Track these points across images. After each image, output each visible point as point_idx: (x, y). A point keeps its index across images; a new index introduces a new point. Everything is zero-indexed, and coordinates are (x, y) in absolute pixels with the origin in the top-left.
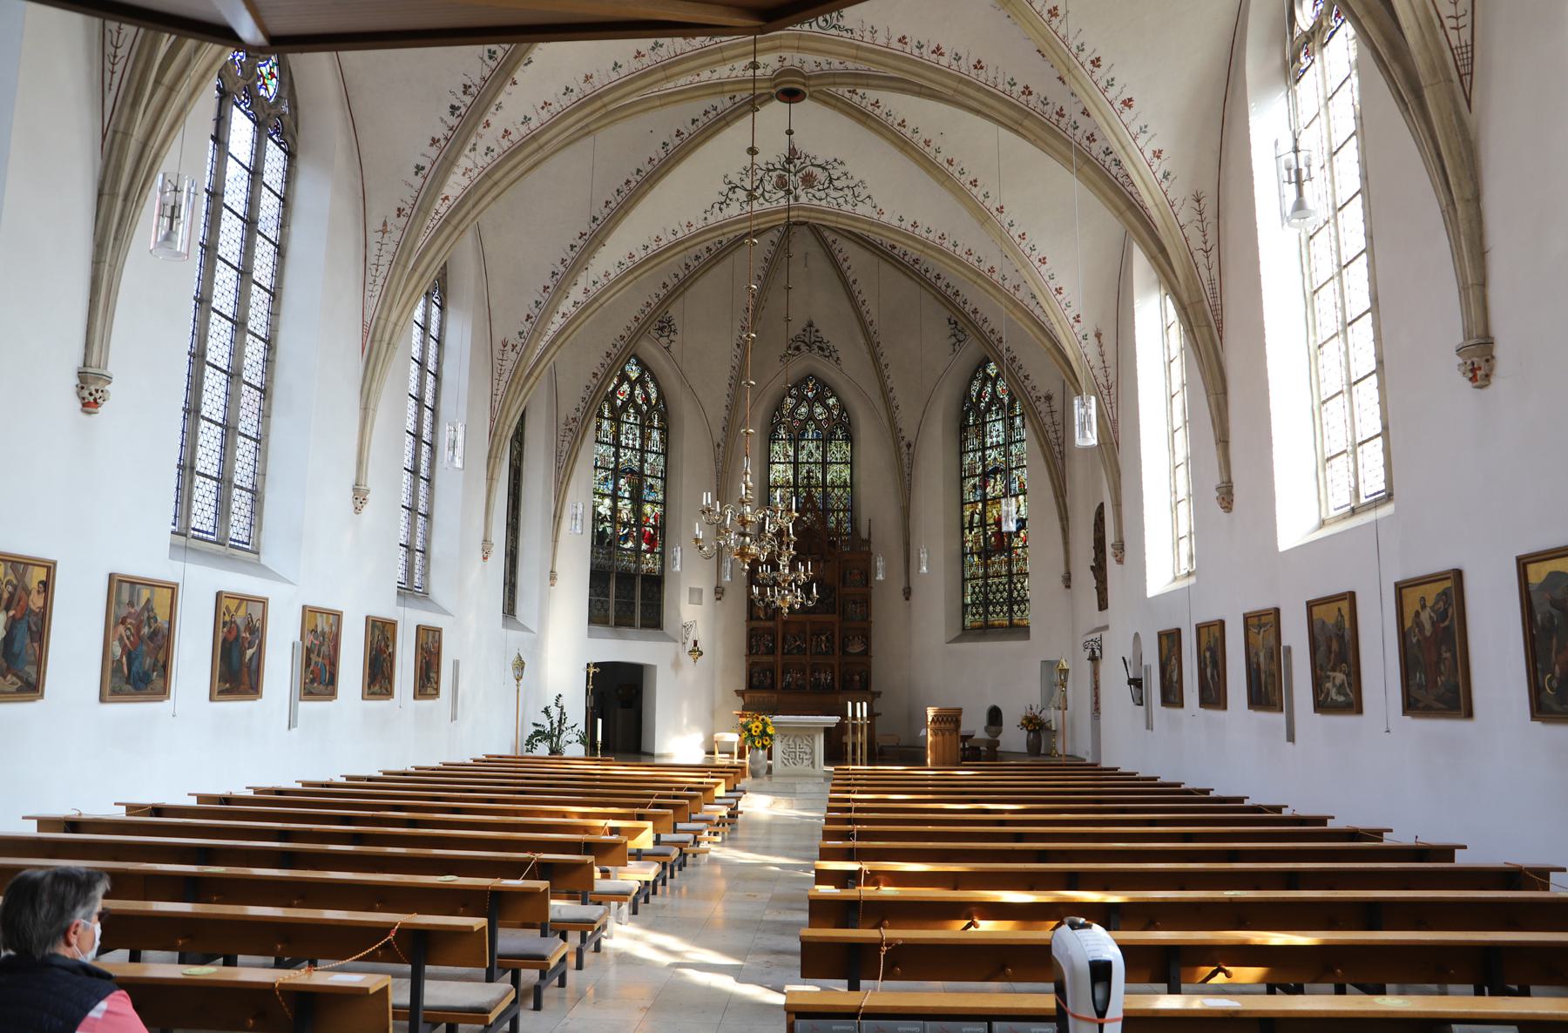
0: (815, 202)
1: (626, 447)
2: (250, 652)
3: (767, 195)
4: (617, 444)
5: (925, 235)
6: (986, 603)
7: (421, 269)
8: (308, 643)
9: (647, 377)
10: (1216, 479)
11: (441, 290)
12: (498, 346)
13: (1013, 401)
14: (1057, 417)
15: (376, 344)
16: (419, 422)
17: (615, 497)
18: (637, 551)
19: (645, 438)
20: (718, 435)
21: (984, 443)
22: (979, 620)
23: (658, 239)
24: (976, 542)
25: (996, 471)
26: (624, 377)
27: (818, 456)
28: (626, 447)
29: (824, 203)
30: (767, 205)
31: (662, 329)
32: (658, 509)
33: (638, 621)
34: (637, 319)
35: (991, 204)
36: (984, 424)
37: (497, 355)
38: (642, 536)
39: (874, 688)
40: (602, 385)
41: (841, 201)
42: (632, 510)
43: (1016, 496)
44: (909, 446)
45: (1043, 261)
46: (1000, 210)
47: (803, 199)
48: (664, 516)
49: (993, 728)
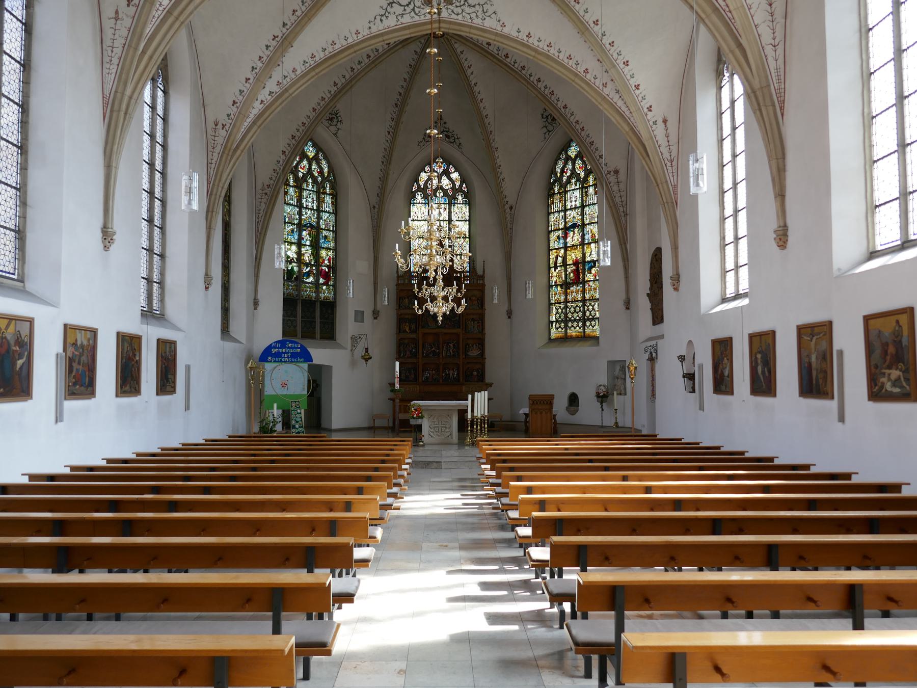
0: (454, 16)
1: (307, 208)
2: (20, 362)
3: (417, 10)
4: (300, 206)
5: (536, 43)
6: (566, 321)
7: (149, 53)
8: (69, 354)
9: (321, 156)
10: (773, 224)
11: (163, 75)
12: (211, 125)
13: (587, 176)
14: (622, 186)
15: (116, 114)
16: (151, 238)
17: (300, 245)
18: (316, 284)
19: (320, 201)
20: (374, 200)
21: (565, 206)
22: (561, 332)
23: (334, 43)
24: (560, 276)
25: (574, 226)
26: (304, 156)
27: (445, 216)
28: (307, 208)
29: (460, 17)
30: (417, 18)
31: (331, 119)
32: (331, 254)
33: (318, 335)
34: (314, 110)
35: (589, 18)
36: (566, 192)
37: (210, 131)
38: (320, 273)
39: (487, 380)
40: (289, 161)
41: (473, 15)
42: (312, 254)
43: (589, 244)
44: (511, 208)
45: (626, 63)
46: (596, 23)
47: (444, 14)
48: (335, 259)
49: (572, 408)
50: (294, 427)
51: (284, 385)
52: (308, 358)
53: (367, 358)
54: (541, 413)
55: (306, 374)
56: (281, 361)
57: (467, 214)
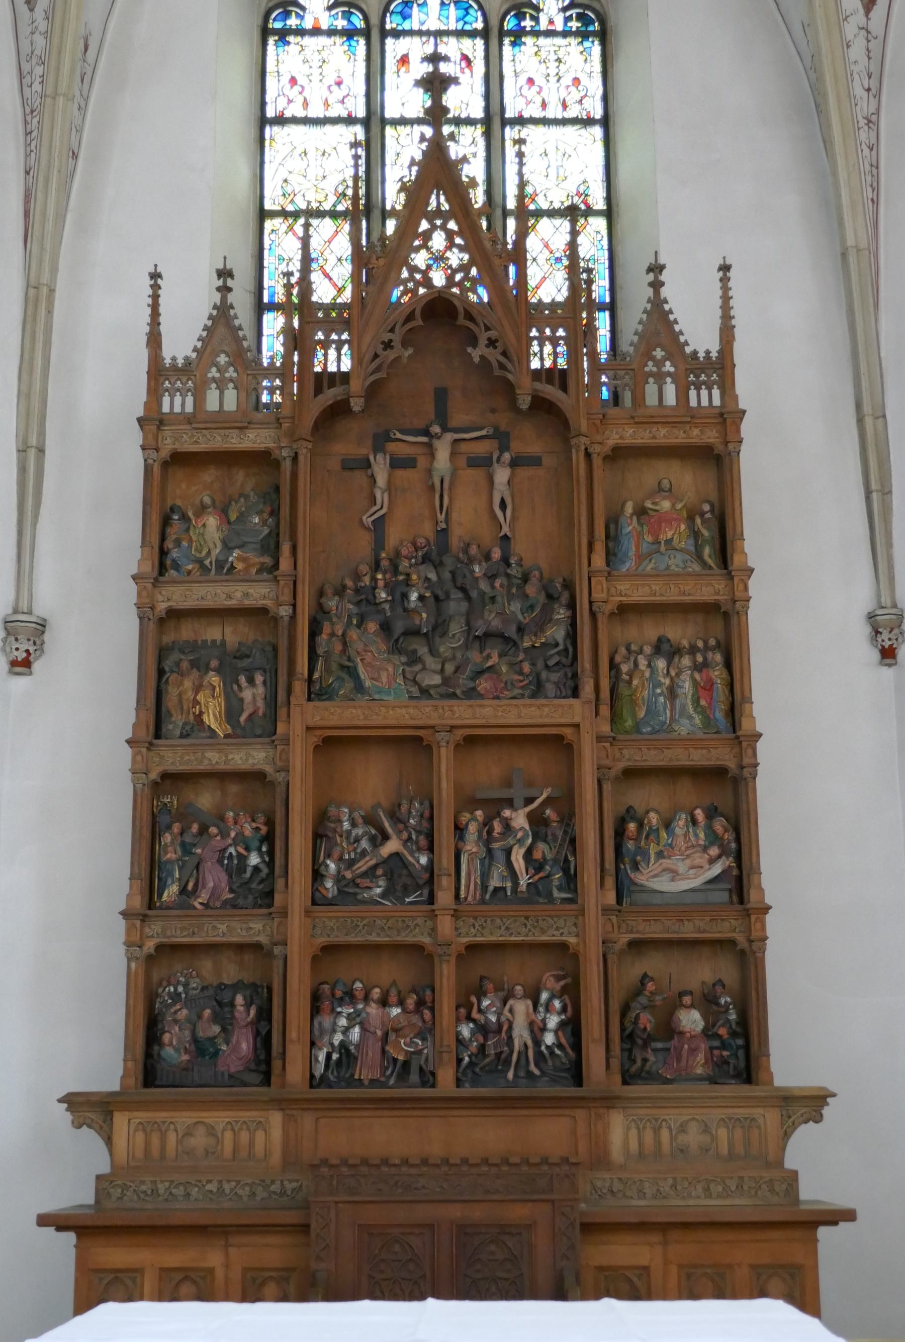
57: (595, 86)
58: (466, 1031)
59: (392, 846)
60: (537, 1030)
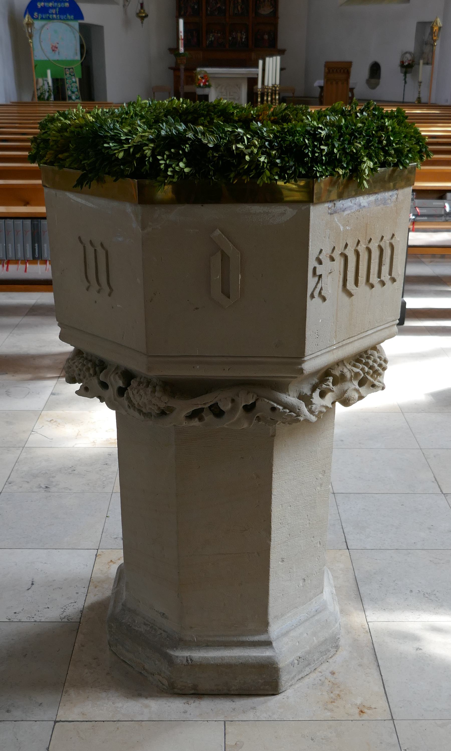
49: (373, 81)
50: (70, 98)
51: (54, 49)
52: (78, 15)
53: (142, 16)
54: (337, 83)
55: (78, 35)
56: (49, 19)
58: (230, 38)
59: (219, 5)
60: (241, 38)
